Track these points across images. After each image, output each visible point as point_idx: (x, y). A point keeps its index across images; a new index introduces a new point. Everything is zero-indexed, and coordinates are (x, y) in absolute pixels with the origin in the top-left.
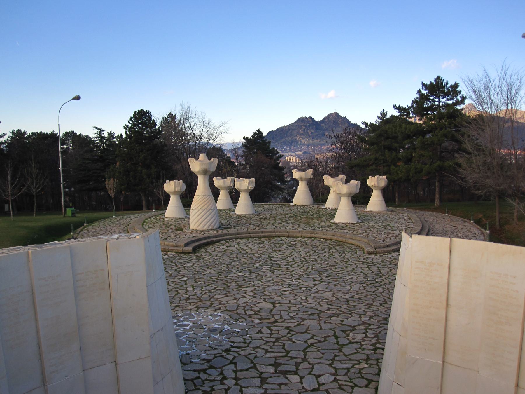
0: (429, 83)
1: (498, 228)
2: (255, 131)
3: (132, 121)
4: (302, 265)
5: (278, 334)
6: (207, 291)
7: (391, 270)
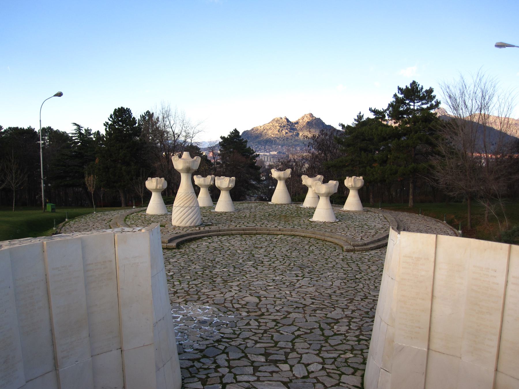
0: (404, 88)
1: (469, 228)
2: (232, 130)
3: (112, 119)
4: (284, 262)
5: (266, 326)
6: (193, 286)
7: (369, 267)
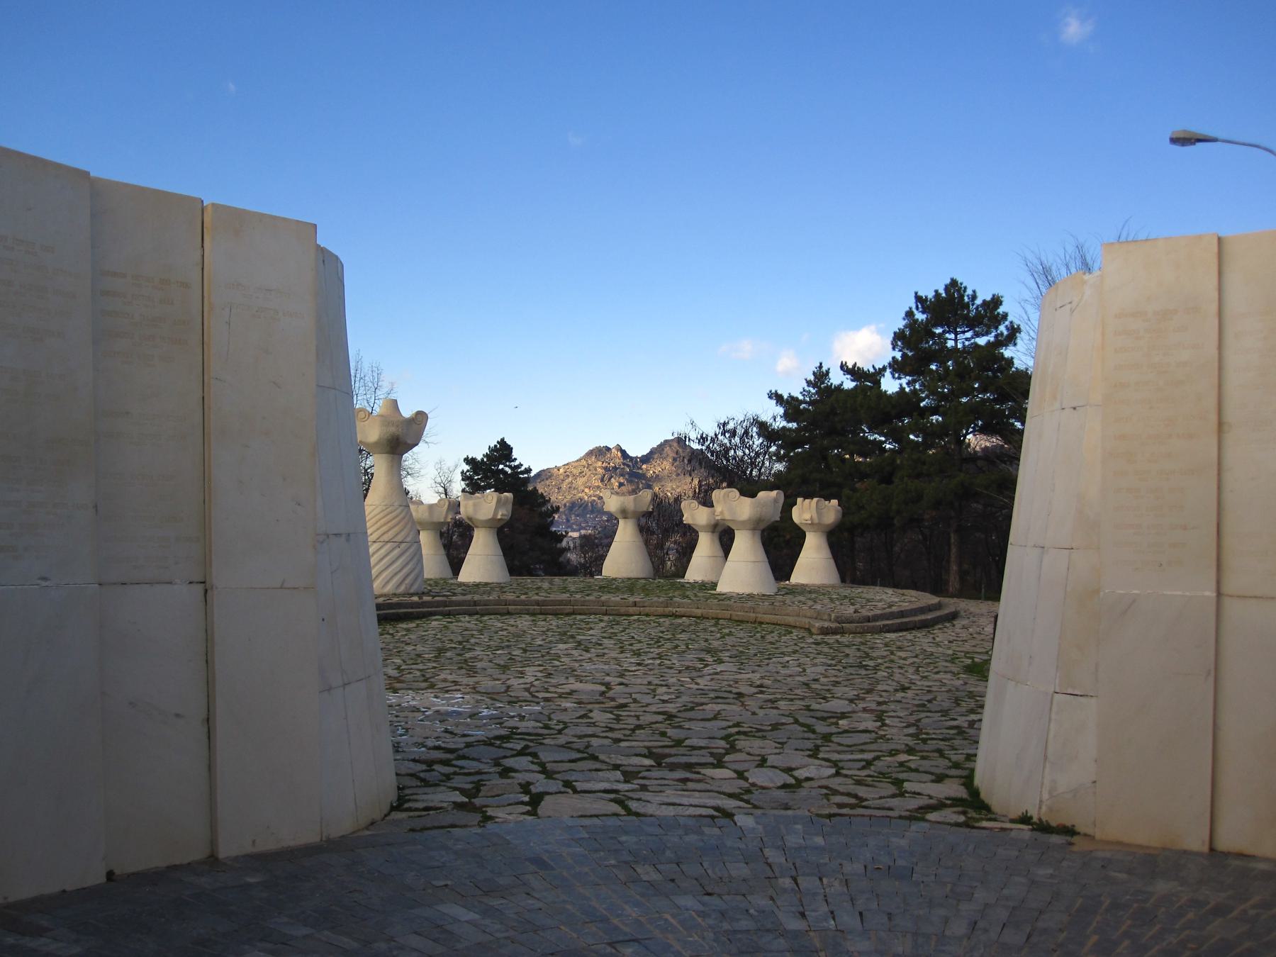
0: (931, 295)
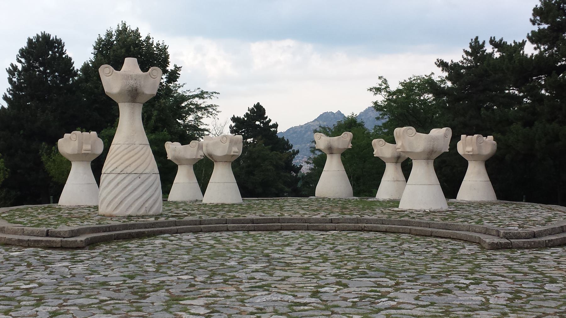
2: (251, 106)
